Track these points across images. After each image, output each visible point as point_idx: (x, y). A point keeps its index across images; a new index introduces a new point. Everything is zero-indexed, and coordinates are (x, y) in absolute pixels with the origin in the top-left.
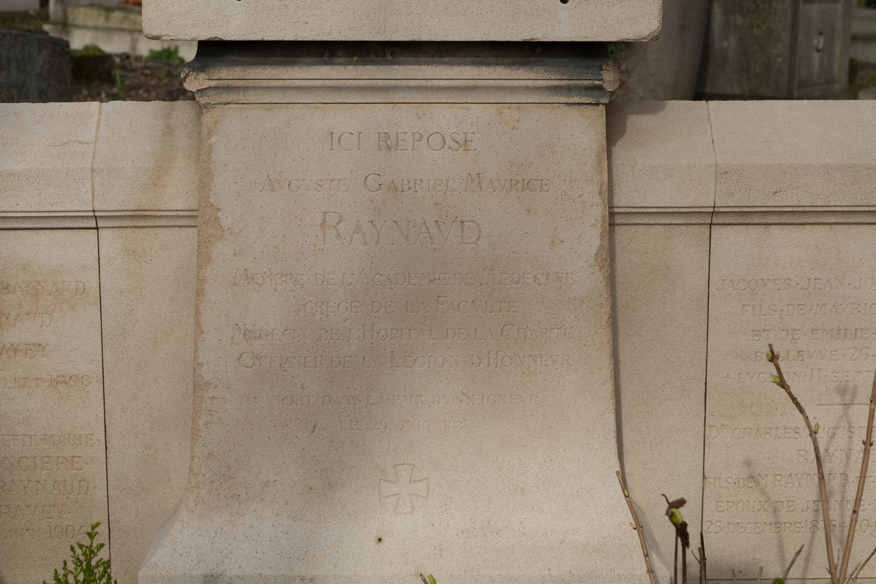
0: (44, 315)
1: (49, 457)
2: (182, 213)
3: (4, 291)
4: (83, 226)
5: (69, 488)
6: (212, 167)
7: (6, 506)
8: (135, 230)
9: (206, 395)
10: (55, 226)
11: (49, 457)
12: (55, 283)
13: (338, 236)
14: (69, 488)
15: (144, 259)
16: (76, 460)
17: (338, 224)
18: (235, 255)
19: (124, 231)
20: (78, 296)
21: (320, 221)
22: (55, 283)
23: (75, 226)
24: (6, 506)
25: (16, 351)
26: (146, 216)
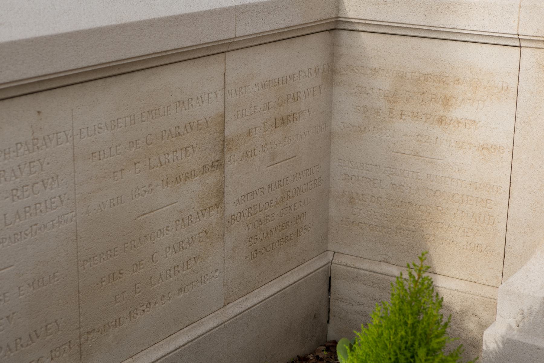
3: (456, 82)
11: (472, 197)
23: (506, 44)
24: (442, 223)
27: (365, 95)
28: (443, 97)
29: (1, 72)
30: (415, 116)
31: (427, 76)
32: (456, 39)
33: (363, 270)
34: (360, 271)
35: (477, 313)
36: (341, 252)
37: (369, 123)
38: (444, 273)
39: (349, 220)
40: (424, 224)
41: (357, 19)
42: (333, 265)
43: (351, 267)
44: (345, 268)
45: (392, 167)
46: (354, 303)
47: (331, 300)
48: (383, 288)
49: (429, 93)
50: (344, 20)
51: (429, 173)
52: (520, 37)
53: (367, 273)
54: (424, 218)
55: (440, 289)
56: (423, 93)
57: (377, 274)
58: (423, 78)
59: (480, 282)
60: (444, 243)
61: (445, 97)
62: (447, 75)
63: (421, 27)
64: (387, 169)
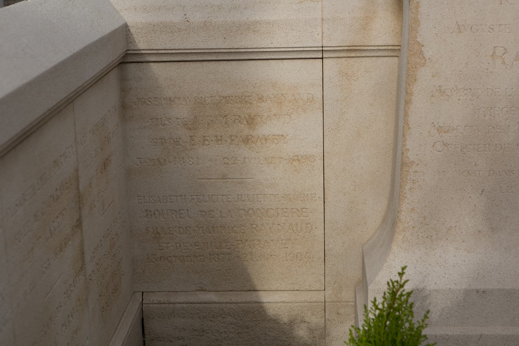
0: (286, 116)
1: (287, 209)
2: (381, 48)
3: (259, 100)
4: (314, 57)
5: (299, 229)
6: (419, 17)
7: (258, 240)
8: (348, 59)
9: (410, 170)
10: (295, 57)
11: (287, 209)
12: (293, 95)
13: (504, 63)
14: (299, 229)
15: (353, 78)
16: (304, 210)
17: (503, 54)
18: (433, 77)
19: (340, 60)
20: (309, 103)
21: (492, 53)
22: (293, 95)
23: (308, 57)
24: (258, 240)
25: (266, 139)
26: (357, 50)
27: (161, 126)
28: (247, 117)
29: (403, 343)
30: (219, 139)
31: (227, 98)
32: (256, 58)
33: (179, 303)
34: (176, 305)
35: (306, 319)
36: (150, 290)
37: (169, 154)
38: (265, 288)
39: (155, 256)
40: (239, 244)
41: (149, 50)
42: (144, 306)
43: (165, 303)
44: (159, 305)
45: (198, 194)
46: (173, 339)
47: (146, 342)
48: (203, 317)
49: (233, 117)
50: (133, 52)
51: (240, 193)
52: (324, 49)
53: (185, 305)
54: (239, 239)
55: (265, 304)
56: (225, 116)
57: (194, 305)
58: (224, 101)
59: (302, 289)
60: (263, 259)
61: (249, 116)
62: (250, 94)
63: (221, 51)
64: (193, 197)
